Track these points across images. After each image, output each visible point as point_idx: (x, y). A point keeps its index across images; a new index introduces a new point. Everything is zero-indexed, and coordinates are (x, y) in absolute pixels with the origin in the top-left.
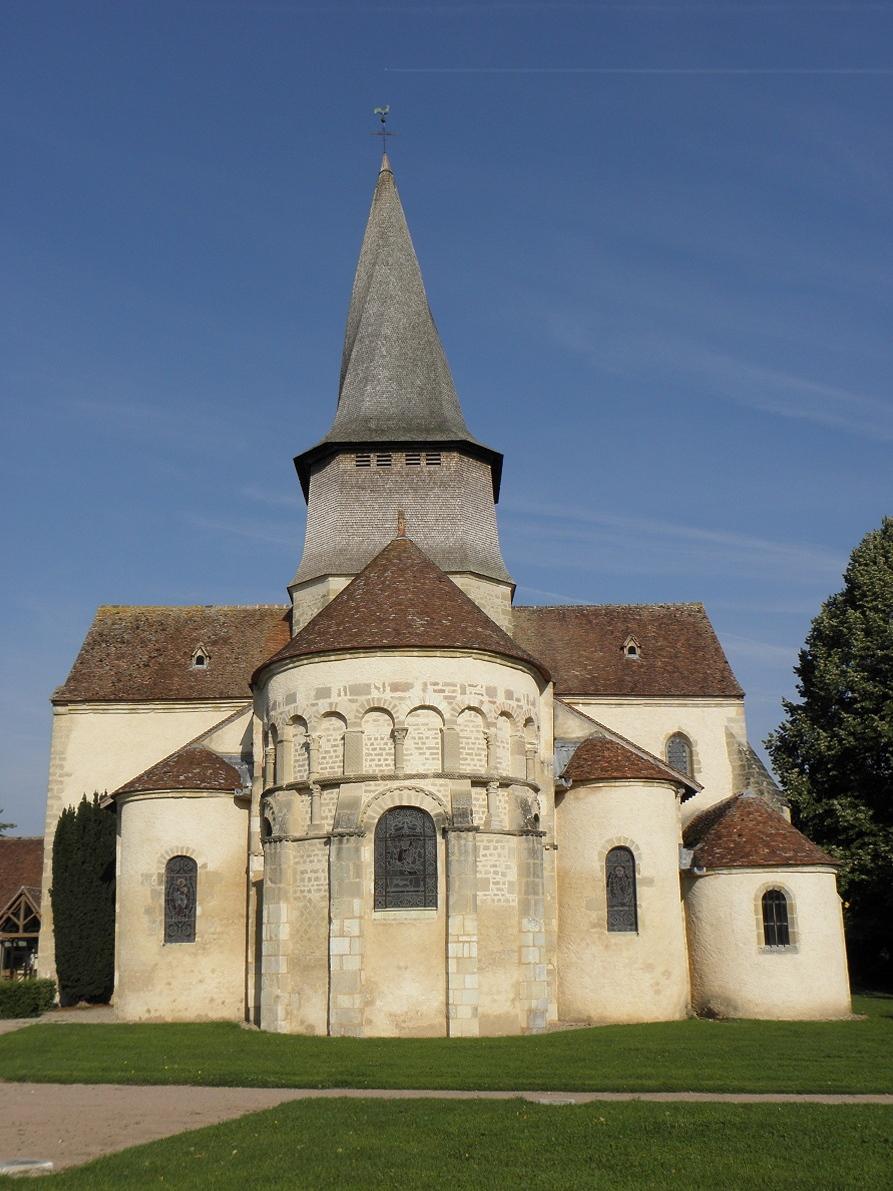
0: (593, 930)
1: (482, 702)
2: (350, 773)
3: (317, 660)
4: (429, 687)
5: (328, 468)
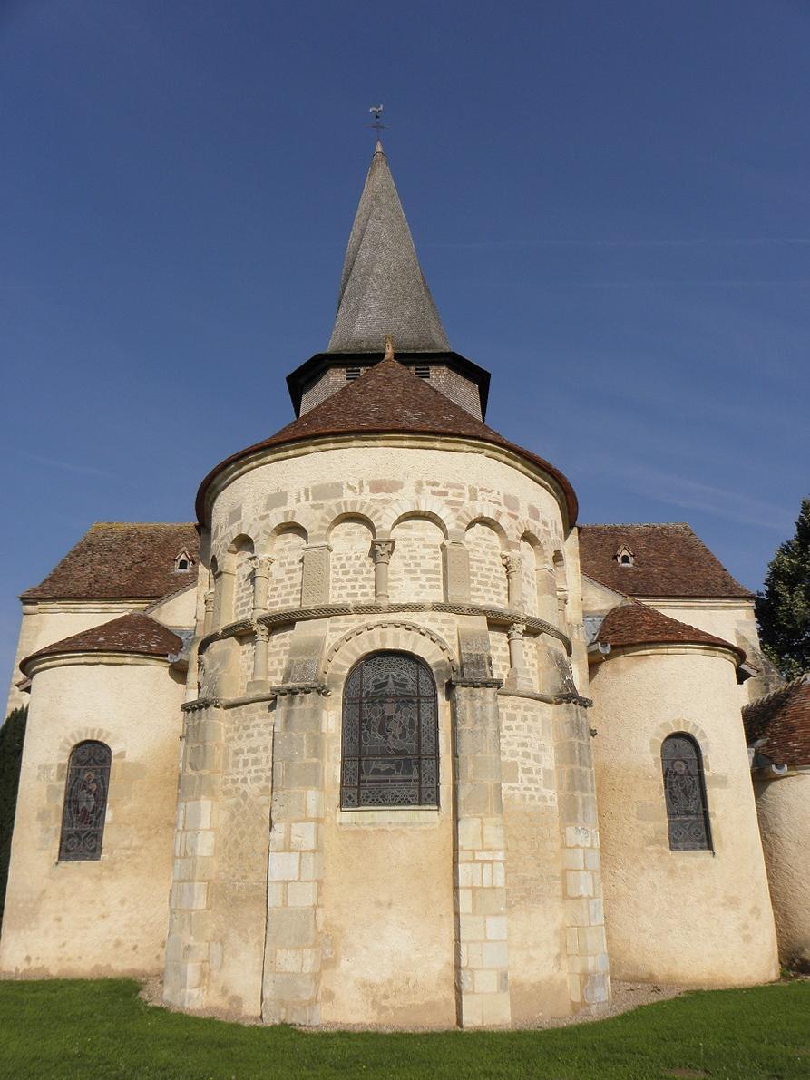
0: (650, 848)
1: (499, 513)
2: (311, 604)
3: (270, 458)
4: (425, 486)
5: (319, 384)
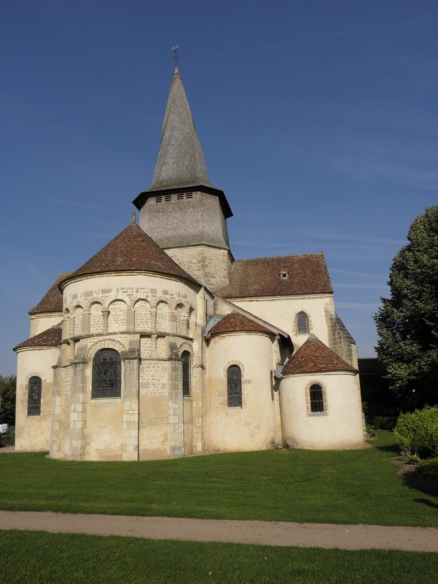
0: (221, 406)
1: (147, 296)
4: (120, 290)
